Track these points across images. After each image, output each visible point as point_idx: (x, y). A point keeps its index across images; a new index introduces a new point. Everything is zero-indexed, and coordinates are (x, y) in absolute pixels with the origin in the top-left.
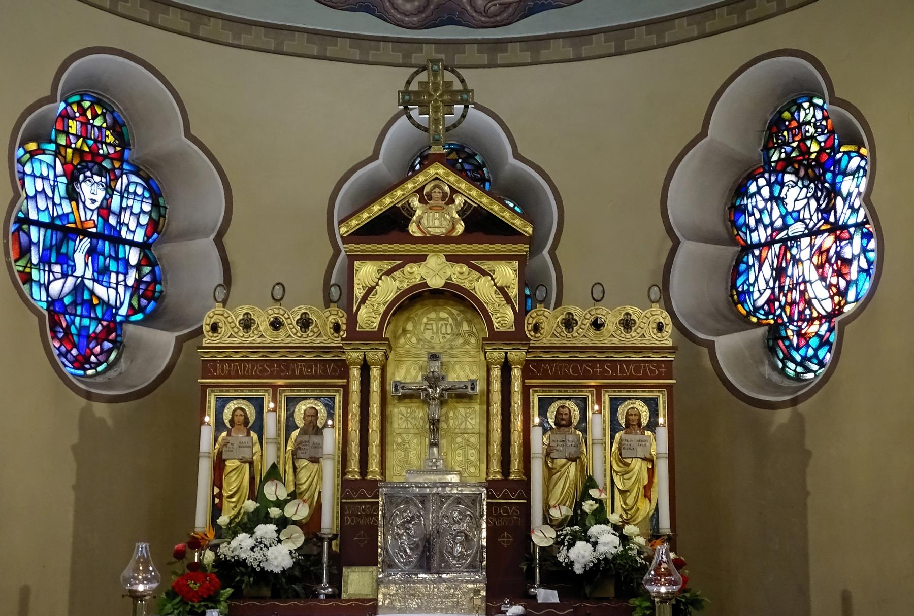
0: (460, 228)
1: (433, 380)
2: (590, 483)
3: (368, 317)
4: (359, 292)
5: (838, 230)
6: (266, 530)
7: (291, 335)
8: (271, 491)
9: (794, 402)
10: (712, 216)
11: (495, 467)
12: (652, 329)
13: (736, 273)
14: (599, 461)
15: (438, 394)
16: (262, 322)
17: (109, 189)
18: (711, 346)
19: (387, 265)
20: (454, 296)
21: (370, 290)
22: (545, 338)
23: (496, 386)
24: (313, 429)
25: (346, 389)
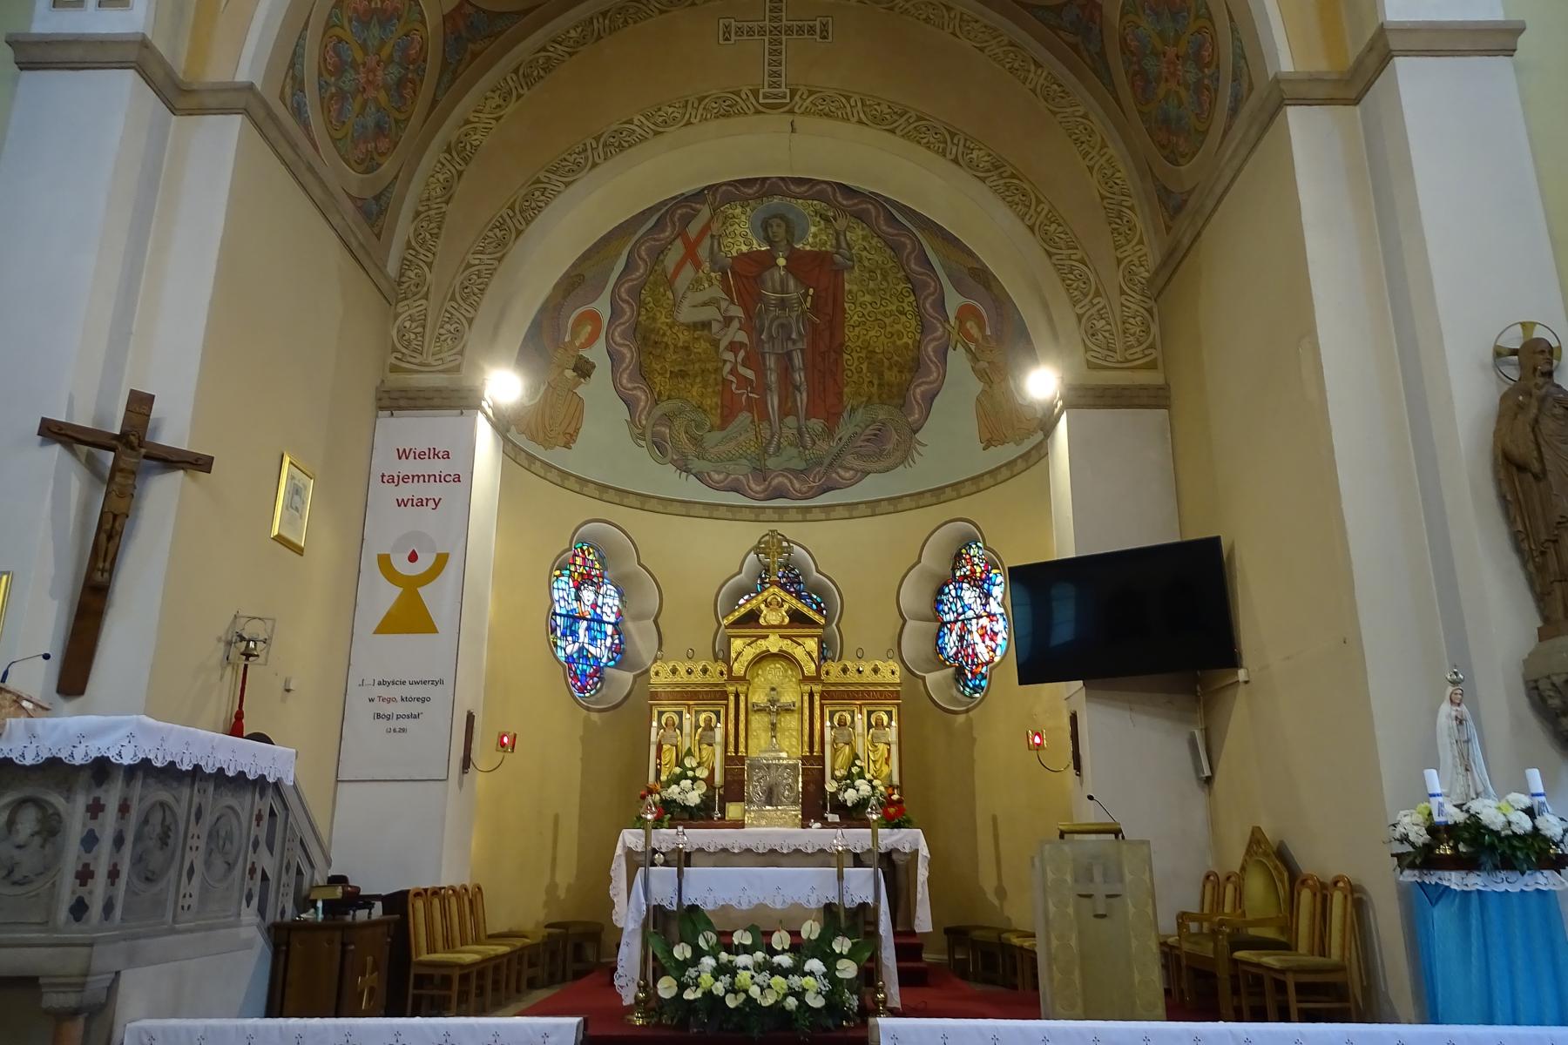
0: (787, 620)
1: (773, 702)
2: (856, 757)
3: (738, 668)
4: (733, 655)
5: (990, 616)
6: (686, 783)
7: (697, 678)
8: (688, 762)
9: (967, 711)
10: (925, 606)
11: (806, 749)
12: (890, 673)
13: (938, 637)
14: (861, 745)
15: (776, 709)
16: (682, 670)
17: (597, 593)
18: (923, 679)
19: (748, 641)
20: (783, 656)
21: (739, 654)
22: (832, 679)
23: (806, 705)
24: (710, 728)
25: (727, 706)
